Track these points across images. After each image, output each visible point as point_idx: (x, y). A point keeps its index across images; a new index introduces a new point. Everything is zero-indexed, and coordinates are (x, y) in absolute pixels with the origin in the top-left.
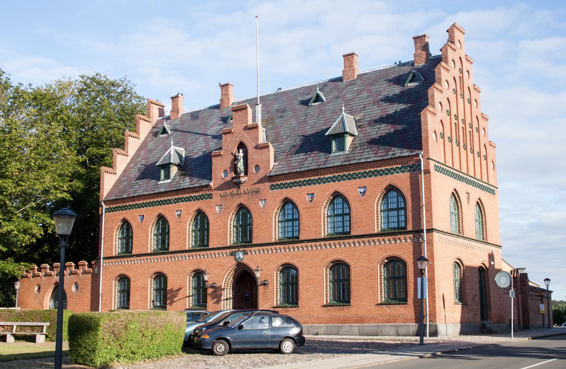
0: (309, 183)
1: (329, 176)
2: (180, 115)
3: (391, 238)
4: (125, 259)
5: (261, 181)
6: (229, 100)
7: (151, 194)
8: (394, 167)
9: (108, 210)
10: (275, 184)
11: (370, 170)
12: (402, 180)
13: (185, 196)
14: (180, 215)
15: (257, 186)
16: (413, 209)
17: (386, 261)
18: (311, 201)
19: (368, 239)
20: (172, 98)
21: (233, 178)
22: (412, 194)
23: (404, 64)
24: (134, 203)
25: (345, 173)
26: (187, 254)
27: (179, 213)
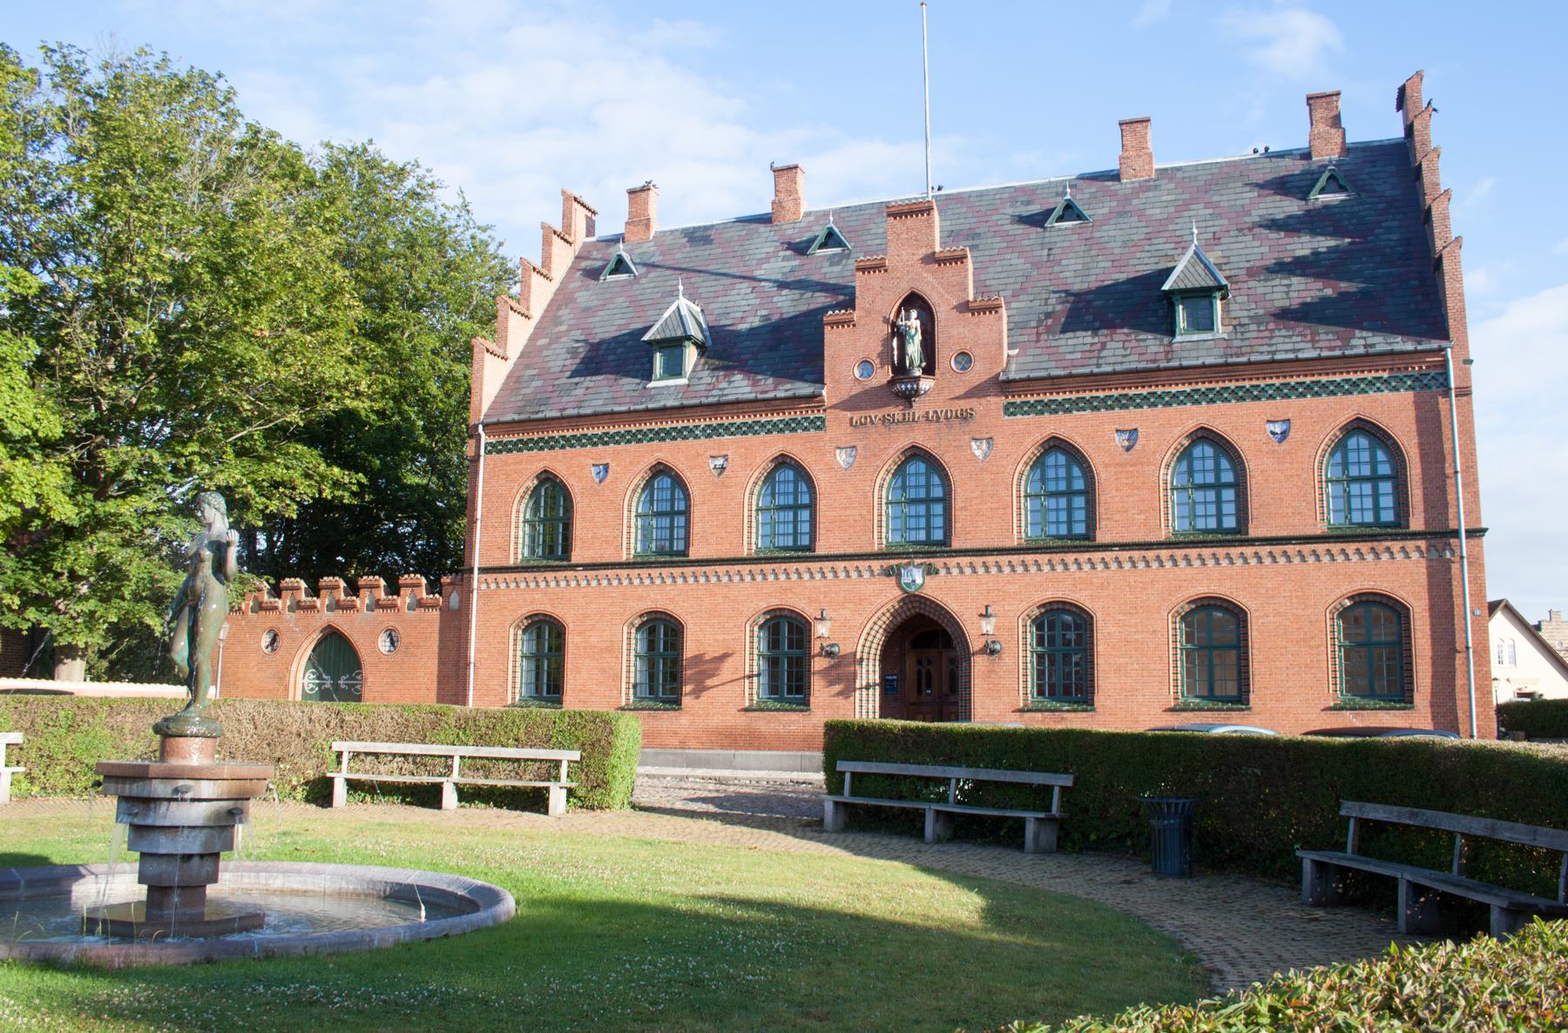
0: (1123, 403)
1: (1180, 388)
2: (652, 234)
3: (1364, 547)
4: (550, 575)
5: (977, 392)
6: (797, 202)
7: (636, 411)
8: (1369, 376)
9: (494, 448)
10: (1018, 400)
11: (1302, 379)
12: (1394, 409)
13: (739, 420)
14: (723, 468)
15: (965, 404)
16: (1426, 479)
17: (1348, 603)
18: (1128, 449)
19: (1298, 547)
20: (632, 192)
21: (892, 383)
22: (1421, 445)
23: (1281, 155)
24: (578, 433)
25: (1227, 384)
26: (745, 569)
27: (720, 462)
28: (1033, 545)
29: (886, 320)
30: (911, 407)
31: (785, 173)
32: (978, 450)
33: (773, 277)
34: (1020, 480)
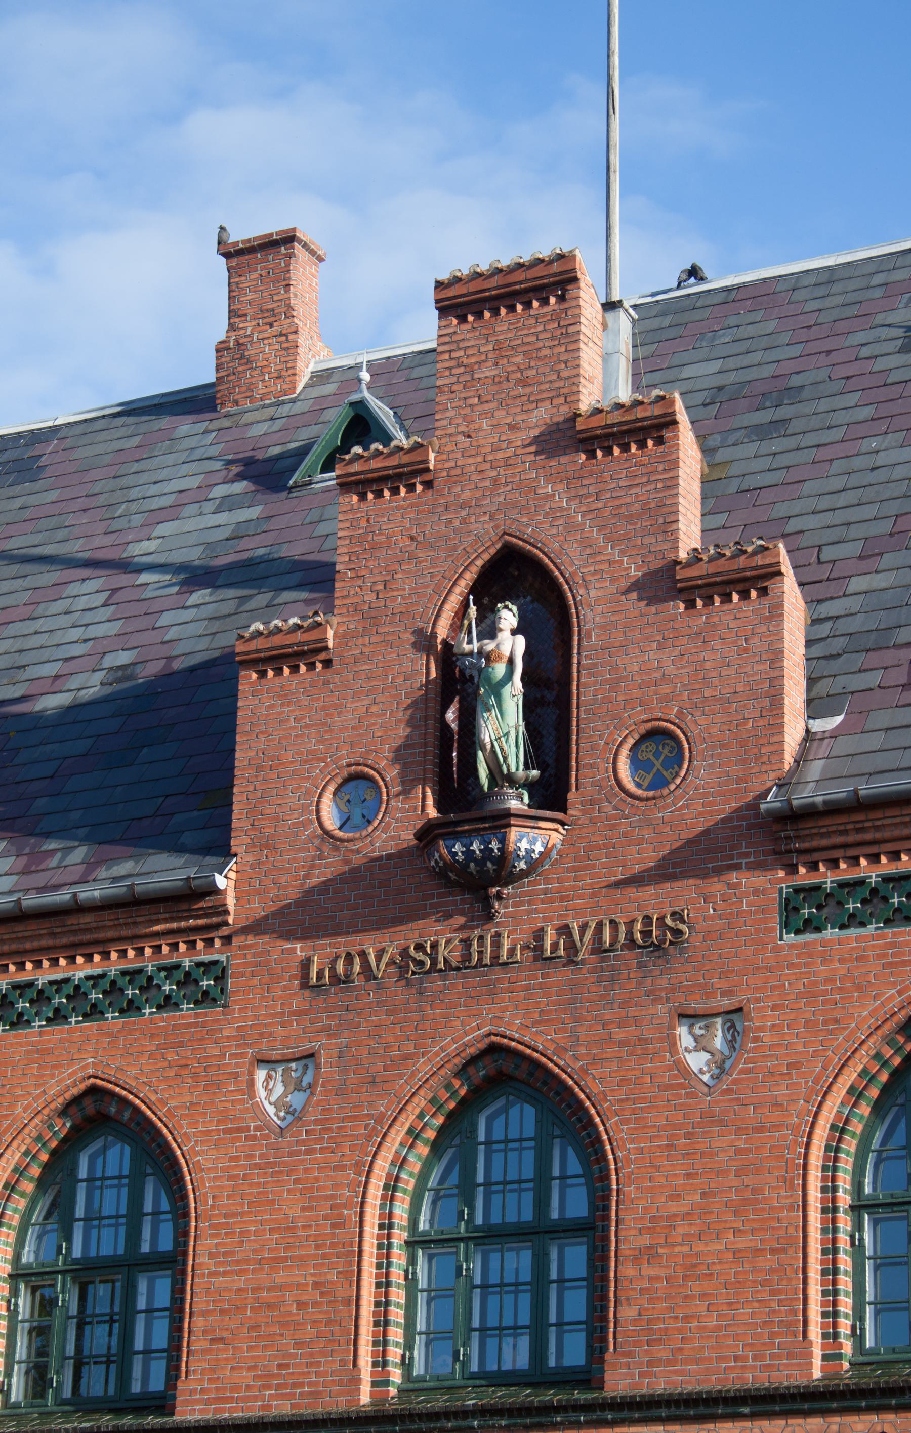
5: (700, 857)
6: (289, 349)
10: (828, 878)
15: (656, 900)
21: (428, 835)
28: (874, 1378)
29: (424, 642)
30: (489, 917)
31: (260, 261)
32: (695, 1054)
33: (177, 557)
34: (833, 1151)
